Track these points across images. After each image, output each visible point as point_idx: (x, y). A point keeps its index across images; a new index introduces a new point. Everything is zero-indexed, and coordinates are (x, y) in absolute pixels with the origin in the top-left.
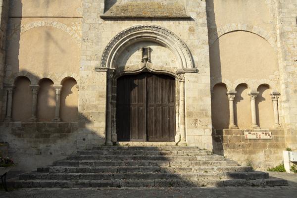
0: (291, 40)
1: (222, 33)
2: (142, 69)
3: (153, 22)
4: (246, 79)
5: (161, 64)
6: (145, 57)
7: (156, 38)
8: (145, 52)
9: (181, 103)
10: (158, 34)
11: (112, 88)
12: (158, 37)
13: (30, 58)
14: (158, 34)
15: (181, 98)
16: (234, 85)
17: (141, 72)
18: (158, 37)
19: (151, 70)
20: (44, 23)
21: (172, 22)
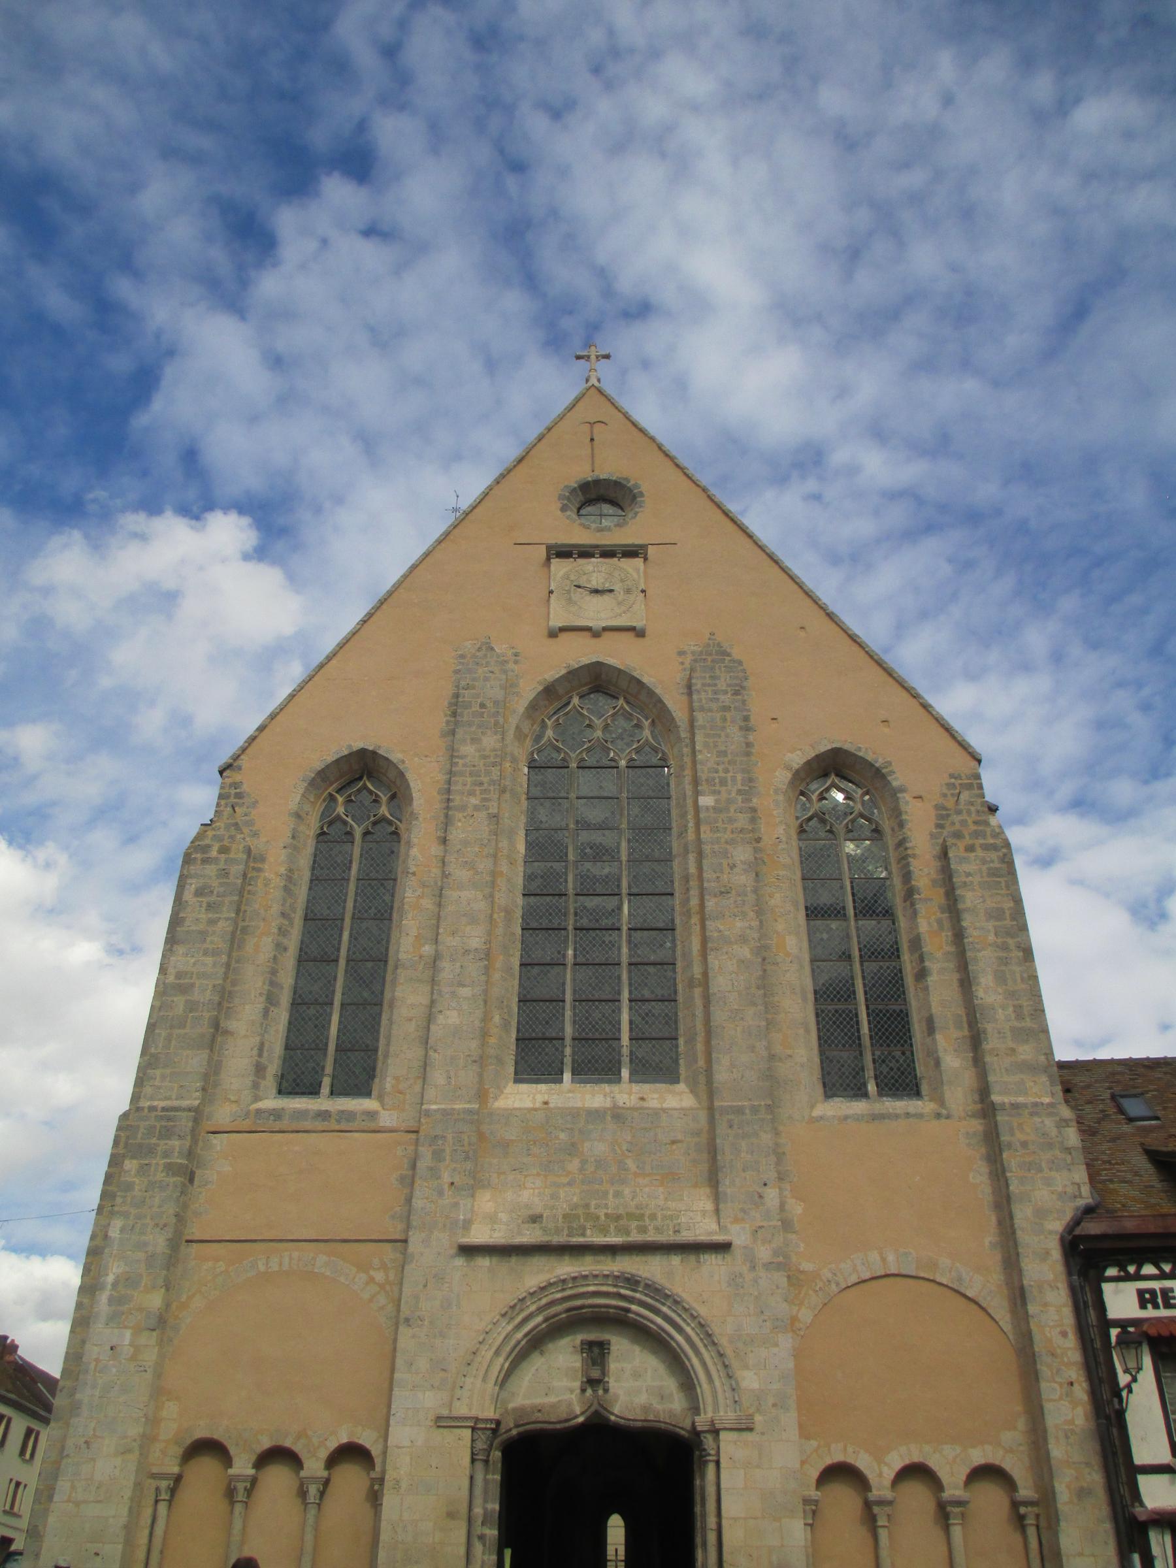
0: (1052, 1309)
1: (838, 1284)
2: (617, 1416)
3: (618, 1258)
4: (927, 1448)
5: (642, 1399)
6: (904, 862)
7: (628, 1310)
8: (596, 1353)
9: (712, 1537)
10: (631, 1300)
11: (486, 1481)
12: (634, 1307)
13: (114, 1370)
14: (631, 1300)
15: (712, 1521)
16: (885, 1469)
17: (583, 1424)
18: (634, 1307)
19: (613, 1418)
20: (286, 1261)
21: (676, 1260)
